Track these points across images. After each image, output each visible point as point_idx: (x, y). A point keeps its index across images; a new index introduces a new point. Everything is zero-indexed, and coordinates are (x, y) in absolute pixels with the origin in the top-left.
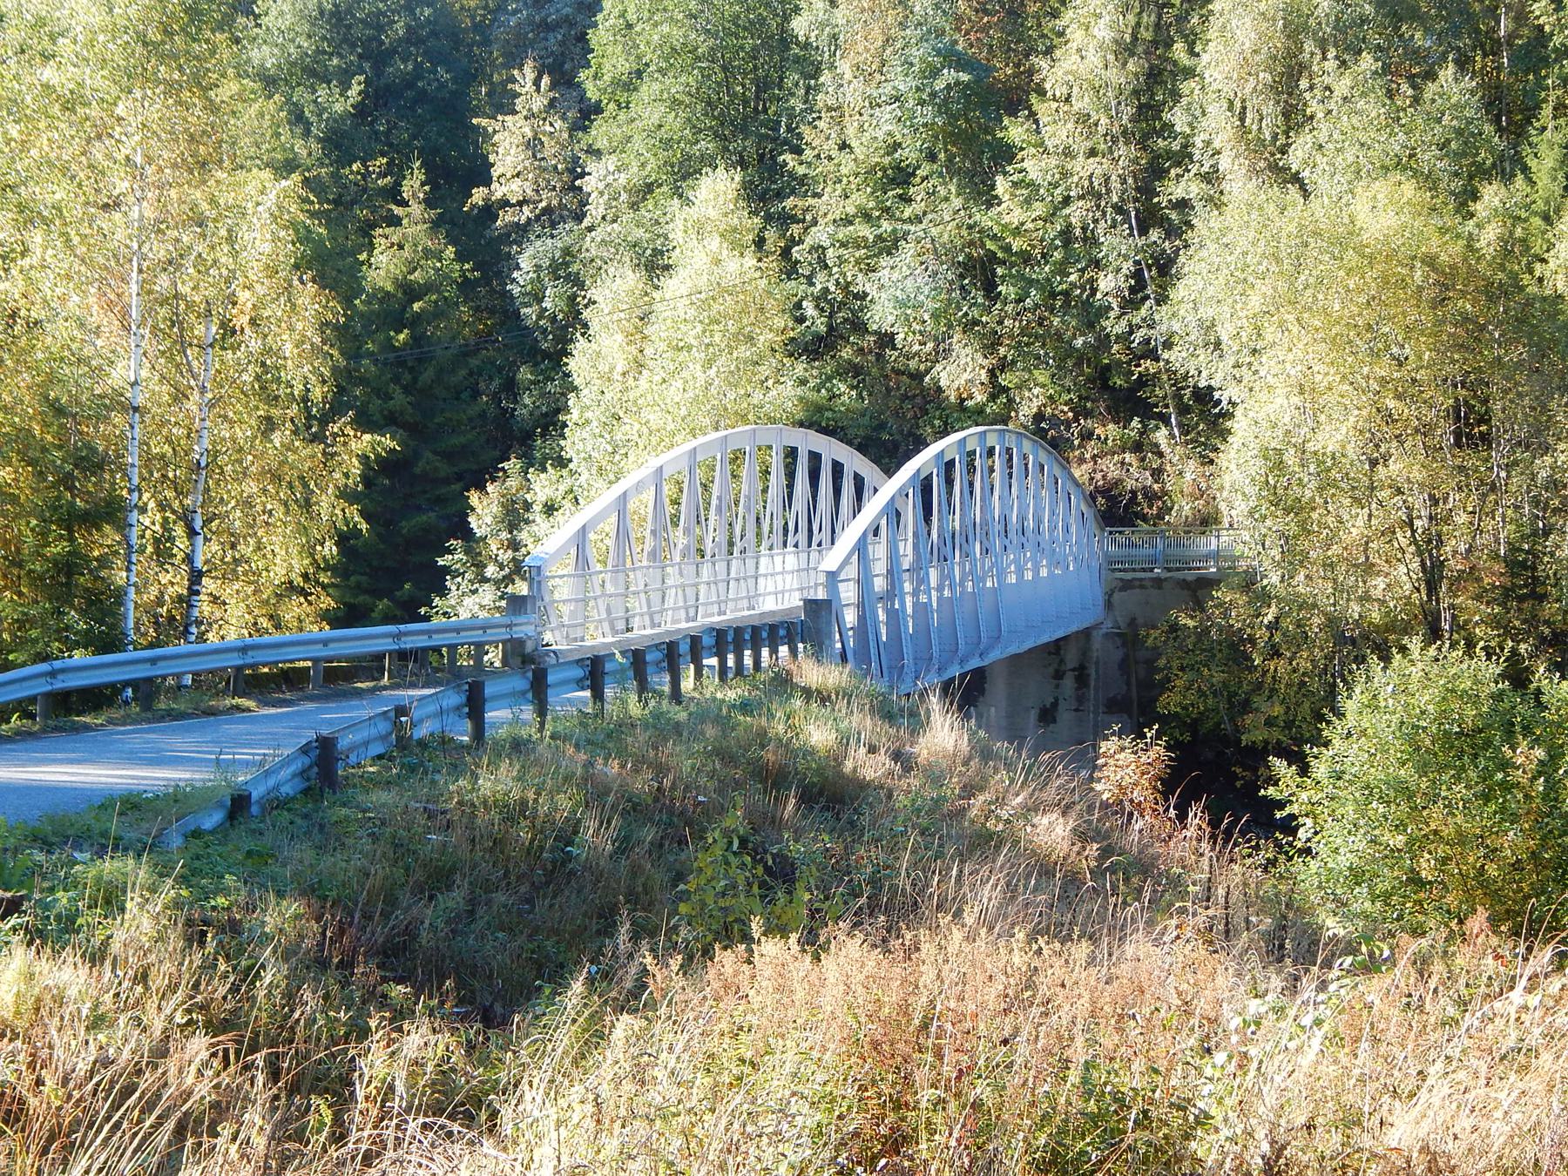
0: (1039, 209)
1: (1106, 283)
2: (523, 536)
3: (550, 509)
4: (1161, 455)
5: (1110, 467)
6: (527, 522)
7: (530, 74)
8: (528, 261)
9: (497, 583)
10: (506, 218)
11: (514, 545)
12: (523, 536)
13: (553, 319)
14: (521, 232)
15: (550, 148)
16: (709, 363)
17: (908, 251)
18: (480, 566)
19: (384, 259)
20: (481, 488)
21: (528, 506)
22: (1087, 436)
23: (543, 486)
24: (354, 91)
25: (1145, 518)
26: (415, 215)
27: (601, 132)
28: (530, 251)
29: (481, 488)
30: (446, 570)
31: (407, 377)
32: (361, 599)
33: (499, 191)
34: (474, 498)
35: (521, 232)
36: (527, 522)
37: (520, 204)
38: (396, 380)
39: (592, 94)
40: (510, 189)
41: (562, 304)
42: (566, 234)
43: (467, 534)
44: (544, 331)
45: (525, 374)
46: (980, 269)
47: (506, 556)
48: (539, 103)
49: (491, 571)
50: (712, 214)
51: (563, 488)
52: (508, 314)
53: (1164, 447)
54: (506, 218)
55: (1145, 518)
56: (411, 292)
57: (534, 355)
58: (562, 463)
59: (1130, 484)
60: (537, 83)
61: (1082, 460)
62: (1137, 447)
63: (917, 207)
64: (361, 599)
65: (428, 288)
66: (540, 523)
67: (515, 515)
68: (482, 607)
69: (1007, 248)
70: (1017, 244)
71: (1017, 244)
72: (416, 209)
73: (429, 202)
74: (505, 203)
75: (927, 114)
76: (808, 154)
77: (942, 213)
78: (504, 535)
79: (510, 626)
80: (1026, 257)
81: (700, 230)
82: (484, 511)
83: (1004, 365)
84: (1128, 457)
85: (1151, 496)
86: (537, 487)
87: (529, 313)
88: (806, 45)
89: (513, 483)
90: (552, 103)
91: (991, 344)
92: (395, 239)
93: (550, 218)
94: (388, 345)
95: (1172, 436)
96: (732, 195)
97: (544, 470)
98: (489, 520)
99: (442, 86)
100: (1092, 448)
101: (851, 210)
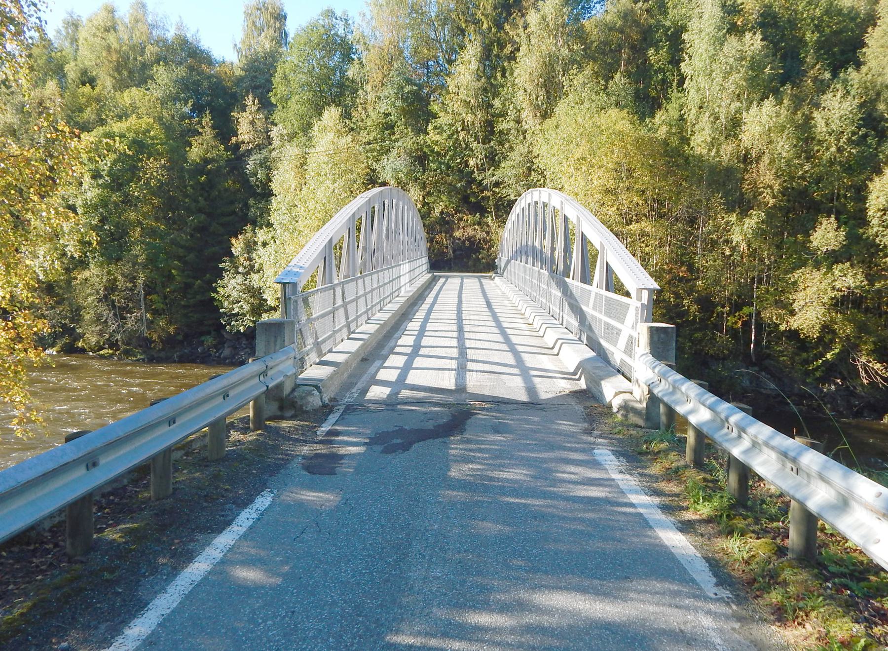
0: (445, 136)
1: (472, 162)
2: (254, 255)
3: (265, 244)
4: (488, 226)
5: (470, 232)
6: (255, 250)
7: (251, 98)
8: (251, 164)
9: (243, 274)
10: (243, 148)
11: (250, 259)
12: (254, 255)
13: (261, 182)
14: (249, 152)
15: (258, 123)
16: (334, 181)
17: (395, 152)
18: (237, 268)
19: (196, 150)
20: (237, 237)
21: (255, 243)
22: (460, 220)
23: (262, 235)
24: (190, 104)
25: (483, 249)
26: (208, 134)
27: (277, 116)
28: (252, 158)
29: (237, 237)
30: (223, 269)
31: (206, 194)
32: (189, 280)
33: (241, 138)
34: (233, 241)
35: (249, 152)
36: (255, 250)
37: (248, 143)
38: (202, 196)
39: (273, 100)
40: (246, 137)
41: (264, 176)
42: (265, 153)
43: (231, 255)
44: (258, 186)
45: (251, 202)
46: (420, 158)
47: (246, 263)
48: (254, 108)
49: (241, 269)
50: (331, 124)
51: (270, 236)
52: (244, 179)
53: (490, 223)
54: (243, 148)
55: (483, 249)
56: (206, 161)
57: (254, 195)
58: (269, 225)
59: (478, 237)
60: (254, 101)
61: (459, 228)
62: (479, 224)
63: (397, 136)
64: (189, 280)
65: (212, 161)
66: (261, 251)
67: (250, 247)
68: (238, 284)
69: (432, 151)
70: (436, 149)
71: (436, 149)
72: (208, 130)
73: (213, 128)
74: (243, 142)
75: (399, 103)
76: (354, 120)
77: (406, 140)
78: (246, 255)
79: (264, 373)
80: (438, 154)
81: (324, 130)
82: (237, 246)
83: (429, 194)
84: (476, 227)
85: (486, 241)
86: (259, 235)
87: (253, 179)
88: (352, 81)
89: (249, 235)
90: (259, 109)
91: (423, 186)
92: (200, 141)
93: (259, 148)
94: (198, 182)
95: (493, 220)
96: (338, 117)
97: (261, 228)
98: (239, 249)
99: (221, 105)
100: (462, 224)
101: (371, 138)
